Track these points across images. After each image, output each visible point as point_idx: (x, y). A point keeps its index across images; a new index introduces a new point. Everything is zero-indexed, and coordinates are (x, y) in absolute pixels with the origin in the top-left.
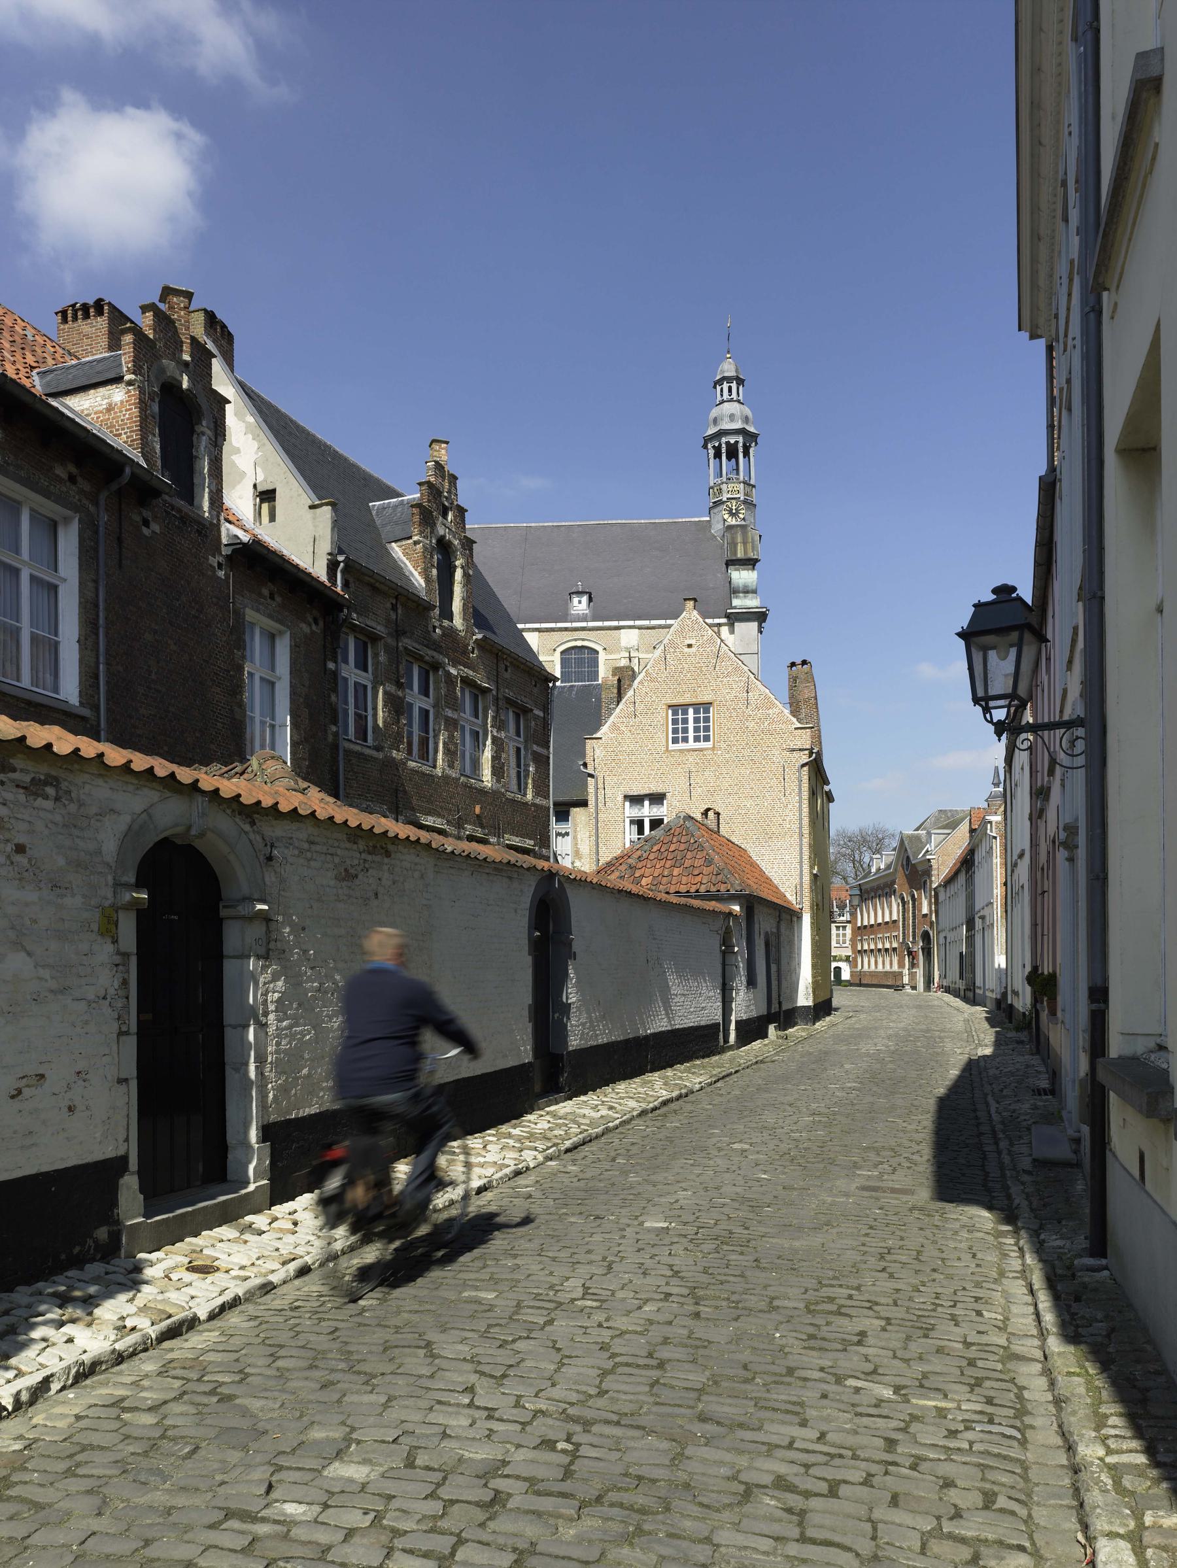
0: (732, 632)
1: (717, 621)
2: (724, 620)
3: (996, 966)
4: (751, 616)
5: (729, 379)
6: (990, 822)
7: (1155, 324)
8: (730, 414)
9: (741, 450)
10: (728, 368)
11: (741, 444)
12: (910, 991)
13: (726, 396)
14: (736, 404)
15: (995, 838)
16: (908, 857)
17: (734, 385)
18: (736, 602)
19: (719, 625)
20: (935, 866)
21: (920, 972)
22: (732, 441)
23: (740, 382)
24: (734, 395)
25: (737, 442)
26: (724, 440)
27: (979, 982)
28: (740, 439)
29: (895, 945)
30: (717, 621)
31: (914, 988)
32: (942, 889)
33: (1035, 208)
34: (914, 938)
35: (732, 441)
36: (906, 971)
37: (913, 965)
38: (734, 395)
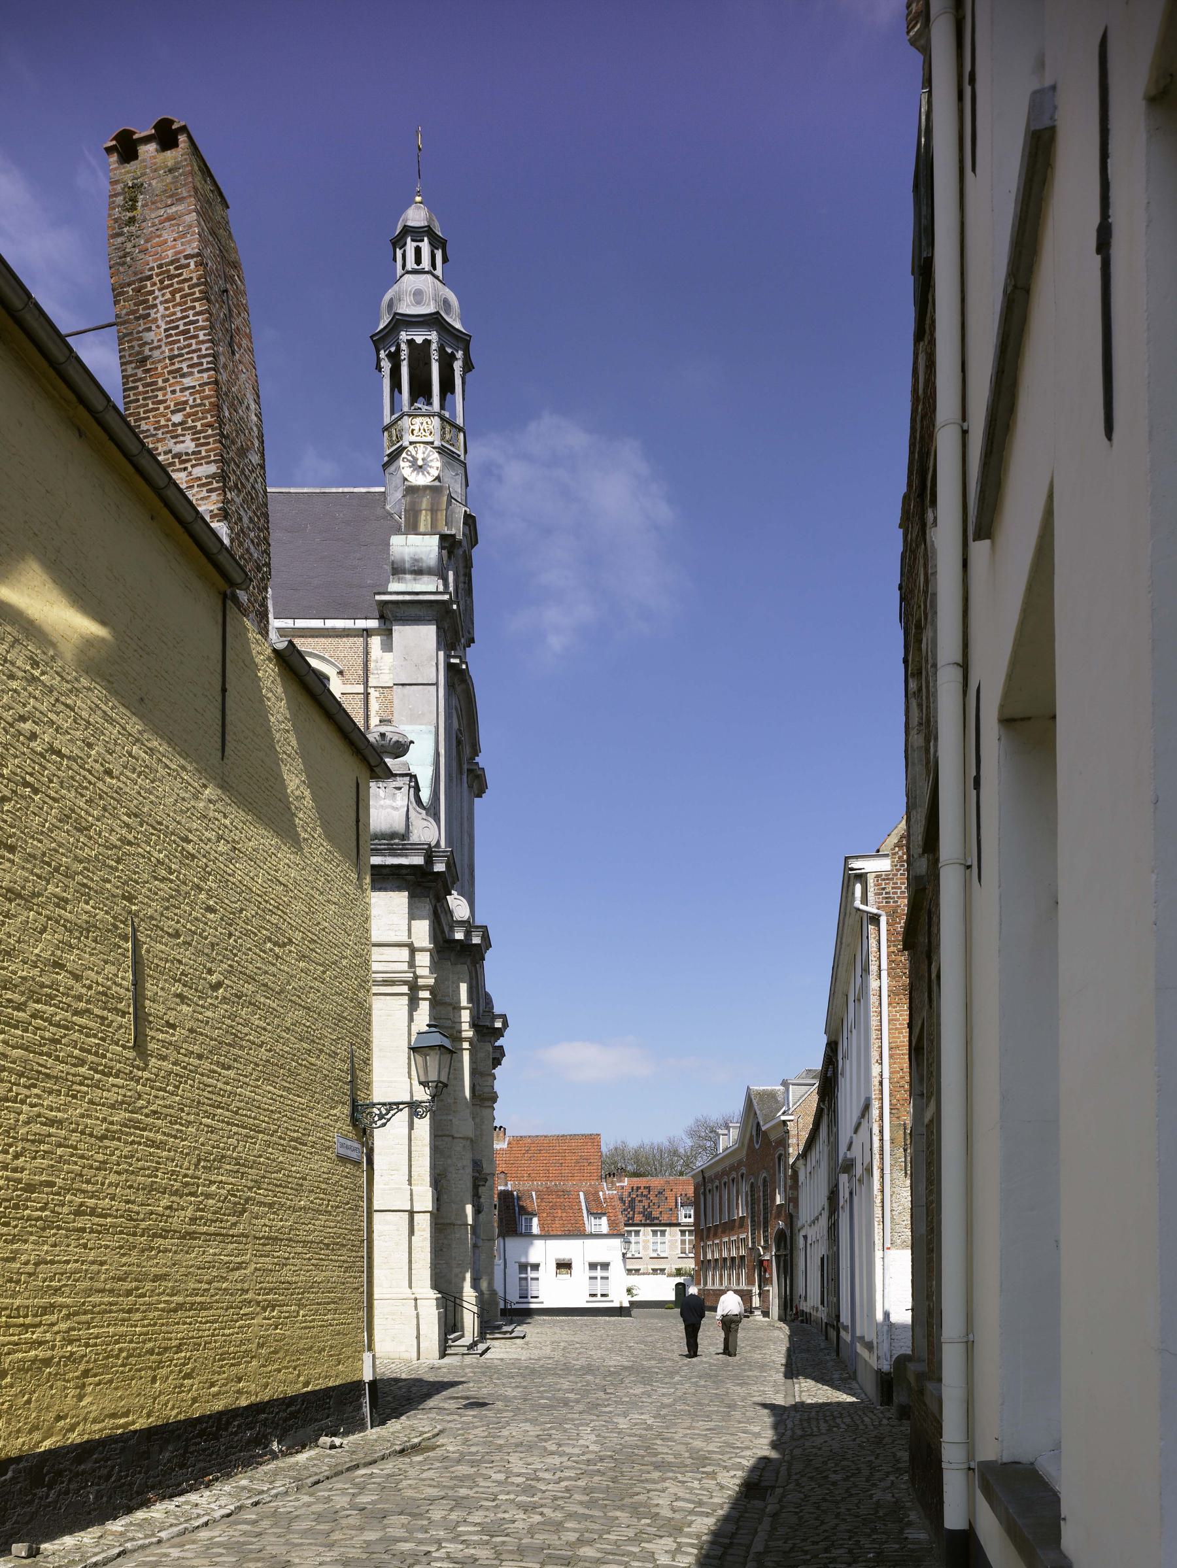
0: (388, 647)
1: (361, 624)
2: (373, 624)
3: (879, 1317)
4: (421, 612)
5: (416, 233)
6: (862, 877)
7: (1048, 482)
8: (418, 290)
9: (435, 356)
10: (416, 216)
11: (434, 346)
12: (761, 1318)
13: (411, 264)
14: (429, 277)
15: (875, 919)
16: (758, 1124)
17: (425, 246)
18: (394, 586)
19: (367, 633)
20: (793, 1132)
21: (773, 1290)
22: (419, 340)
23: (438, 242)
24: (426, 263)
25: (427, 343)
26: (404, 336)
27: (845, 1318)
28: (433, 336)
29: (742, 1252)
30: (361, 624)
31: (766, 1314)
32: (801, 1162)
33: (915, 438)
34: (766, 1241)
35: (419, 340)
36: (756, 1290)
37: (763, 1281)
38: (426, 263)
